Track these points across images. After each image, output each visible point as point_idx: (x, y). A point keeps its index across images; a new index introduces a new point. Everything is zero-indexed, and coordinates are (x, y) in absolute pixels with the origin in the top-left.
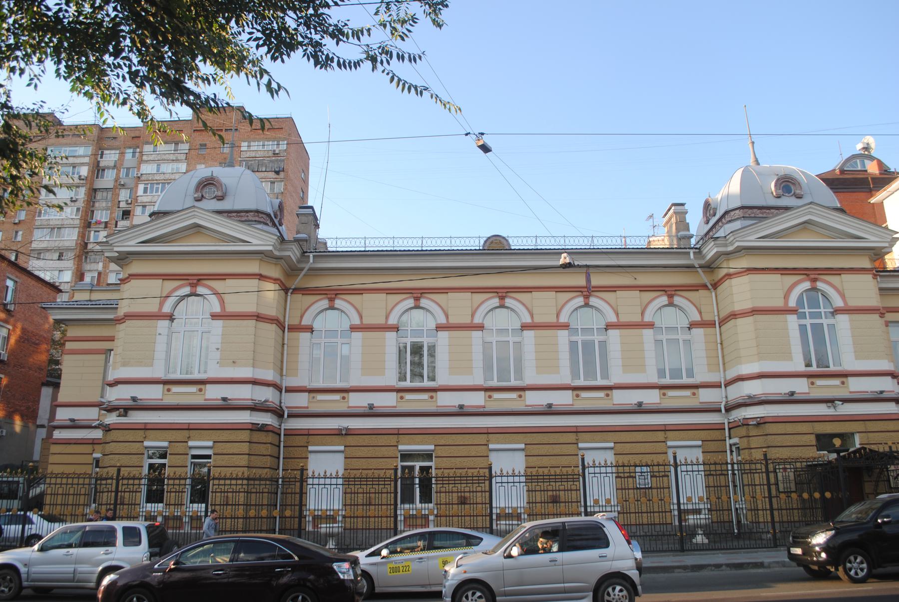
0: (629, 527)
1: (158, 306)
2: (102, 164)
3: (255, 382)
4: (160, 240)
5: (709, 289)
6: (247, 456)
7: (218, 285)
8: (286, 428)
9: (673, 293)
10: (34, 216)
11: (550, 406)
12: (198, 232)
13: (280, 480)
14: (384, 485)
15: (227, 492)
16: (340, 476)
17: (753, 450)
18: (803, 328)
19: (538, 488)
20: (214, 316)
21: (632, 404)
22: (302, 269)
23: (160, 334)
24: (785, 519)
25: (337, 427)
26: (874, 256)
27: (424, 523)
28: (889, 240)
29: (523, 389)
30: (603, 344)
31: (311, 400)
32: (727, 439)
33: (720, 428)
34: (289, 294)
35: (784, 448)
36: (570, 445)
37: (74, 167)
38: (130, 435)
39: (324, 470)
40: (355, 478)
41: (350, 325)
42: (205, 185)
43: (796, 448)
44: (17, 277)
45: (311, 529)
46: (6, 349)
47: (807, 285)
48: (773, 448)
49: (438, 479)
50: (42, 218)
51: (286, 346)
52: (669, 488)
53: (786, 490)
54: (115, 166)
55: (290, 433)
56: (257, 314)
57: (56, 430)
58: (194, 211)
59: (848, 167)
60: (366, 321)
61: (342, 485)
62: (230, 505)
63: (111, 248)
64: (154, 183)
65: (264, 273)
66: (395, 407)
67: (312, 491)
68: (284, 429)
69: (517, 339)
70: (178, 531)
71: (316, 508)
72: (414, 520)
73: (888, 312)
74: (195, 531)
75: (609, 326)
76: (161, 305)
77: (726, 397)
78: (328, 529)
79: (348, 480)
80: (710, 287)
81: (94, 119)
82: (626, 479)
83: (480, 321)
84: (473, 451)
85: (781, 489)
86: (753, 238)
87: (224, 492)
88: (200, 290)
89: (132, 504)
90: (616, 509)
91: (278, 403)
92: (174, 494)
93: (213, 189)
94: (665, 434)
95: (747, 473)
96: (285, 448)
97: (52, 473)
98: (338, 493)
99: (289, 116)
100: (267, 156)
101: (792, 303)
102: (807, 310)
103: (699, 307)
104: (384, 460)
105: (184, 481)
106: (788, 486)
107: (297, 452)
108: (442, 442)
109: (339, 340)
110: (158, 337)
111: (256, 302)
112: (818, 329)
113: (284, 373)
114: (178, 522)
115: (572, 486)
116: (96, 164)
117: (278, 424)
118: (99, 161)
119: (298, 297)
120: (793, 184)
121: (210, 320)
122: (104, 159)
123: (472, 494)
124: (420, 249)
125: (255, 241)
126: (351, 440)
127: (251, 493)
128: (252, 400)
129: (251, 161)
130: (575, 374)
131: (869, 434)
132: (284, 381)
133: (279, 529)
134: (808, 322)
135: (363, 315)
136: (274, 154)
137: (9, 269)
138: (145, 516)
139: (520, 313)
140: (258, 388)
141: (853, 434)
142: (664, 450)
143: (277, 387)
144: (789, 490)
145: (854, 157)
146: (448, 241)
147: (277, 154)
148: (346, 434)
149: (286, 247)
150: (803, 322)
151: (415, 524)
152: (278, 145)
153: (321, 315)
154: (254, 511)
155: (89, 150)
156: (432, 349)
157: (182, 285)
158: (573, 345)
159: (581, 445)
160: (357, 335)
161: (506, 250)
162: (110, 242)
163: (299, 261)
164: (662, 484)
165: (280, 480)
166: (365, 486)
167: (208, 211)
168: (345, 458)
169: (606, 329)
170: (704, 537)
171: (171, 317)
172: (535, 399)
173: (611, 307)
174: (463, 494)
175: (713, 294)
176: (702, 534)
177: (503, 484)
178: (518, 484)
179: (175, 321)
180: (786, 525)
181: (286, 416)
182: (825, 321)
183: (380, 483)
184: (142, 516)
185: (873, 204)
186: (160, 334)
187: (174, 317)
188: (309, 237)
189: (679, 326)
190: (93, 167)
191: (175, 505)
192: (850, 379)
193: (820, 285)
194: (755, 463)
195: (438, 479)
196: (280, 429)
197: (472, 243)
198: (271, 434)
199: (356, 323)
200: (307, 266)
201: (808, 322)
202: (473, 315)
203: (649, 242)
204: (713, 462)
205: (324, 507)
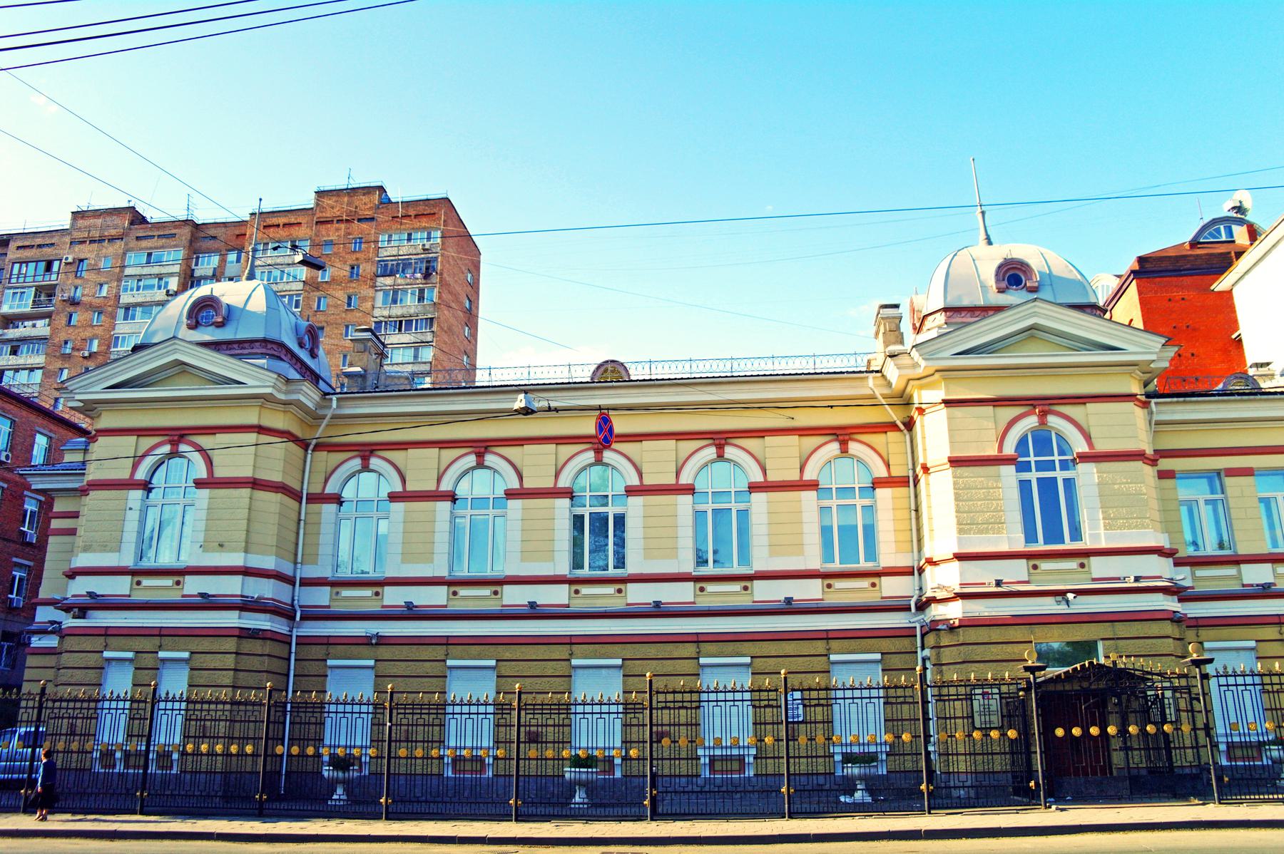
0: (213, 775)
1: (129, 471)
2: (197, 274)
3: (246, 572)
4: (134, 384)
5: (901, 431)
6: (232, 672)
7: (204, 441)
8: (299, 634)
9: (723, 442)
10: (109, 347)
11: (789, 601)
12: (184, 371)
13: (289, 706)
14: (437, 714)
15: (205, 720)
16: (490, 702)
17: (944, 667)
18: (1024, 486)
19: (550, 722)
20: (199, 484)
21: (1252, 585)
22: (323, 417)
23: (131, 509)
24: (980, 768)
25: (364, 634)
26: (1141, 375)
27: (607, 768)
28: (1157, 350)
29: (878, 574)
30: (744, 514)
31: (335, 597)
32: (919, 650)
33: (908, 633)
34: (310, 452)
35: (987, 664)
36: (687, 661)
37: (160, 279)
38: (87, 644)
39: (165, 692)
40: (542, 705)
41: (626, 487)
42: (202, 307)
43: (1004, 664)
44: (51, 431)
45: (450, 774)
46: (37, 527)
47: (1032, 421)
48: (970, 665)
49: (628, 706)
50: (119, 349)
51: (302, 523)
52: (832, 722)
53: (983, 726)
54: (214, 275)
55: (304, 641)
56: (252, 480)
57: (35, 635)
58: (174, 344)
59: (1206, 238)
60: (648, 481)
61: (494, 714)
62: (207, 737)
63: (72, 395)
64: (292, 295)
65: (267, 422)
66: (446, 606)
67: (453, 722)
68: (297, 636)
69: (867, 502)
70: (478, 776)
71: (590, 745)
72: (729, 763)
73: (1161, 457)
74: (160, 772)
75: (877, 483)
76: (135, 467)
77: (921, 589)
78: (573, 774)
79: (629, 708)
80: (902, 427)
81: (186, 213)
82: (677, 711)
83: (690, 482)
84: (550, 668)
85: (977, 725)
86: (98, 388)
87: (201, 720)
88: (183, 448)
89: (85, 735)
90: (884, 749)
91: (289, 601)
92: (138, 721)
93: (212, 313)
94: (828, 643)
95: (961, 700)
96: (298, 662)
97: (29, 693)
98: (487, 725)
99: (444, 196)
100: (415, 252)
101: (1009, 449)
102: (1032, 459)
103: (886, 458)
104: (427, 680)
105: (200, 705)
106: (988, 719)
107: (313, 668)
108: (507, 655)
109: (491, 512)
110: (128, 512)
111: (252, 463)
112: (1048, 486)
113: (299, 560)
114: (479, 764)
115: (312, 719)
116: (189, 273)
117: (288, 629)
118: (194, 270)
119: (322, 455)
120: (1024, 272)
121: (194, 489)
122: (199, 267)
123: (672, 728)
124: (729, 374)
125: (1130, 348)
126: (385, 652)
127: (631, 725)
128: (242, 596)
129: (392, 260)
130: (828, 556)
131: (1119, 641)
132: (298, 571)
133: (286, 771)
134: (1033, 476)
135: (407, 479)
136: (424, 250)
137: (40, 420)
138: (158, 752)
139: (748, 470)
140: (251, 580)
141: (1095, 642)
142: (825, 667)
143: (290, 580)
144: (988, 726)
145: (1215, 222)
146: (687, 365)
147: (427, 250)
148: (376, 644)
149: (294, 387)
150: (1025, 476)
151: (729, 768)
152: (429, 238)
153: (583, 474)
154: (636, 751)
155: (181, 254)
156: (620, 521)
157: (1025, 412)
158: (699, 515)
159: (703, 661)
160: (399, 507)
161: (625, 381)
162: (70, 388)
163: (319, 406)
164: (899, 713)
165: (289, 706)
166: (410, 716)
167: (190, 342)
168: (376, 676)
169: (874, 488)
170: (865, 794)
171: (147, 486)
172: (766, 592)
173: (757, 461)
174: (660, 728)
175: (908, 437)
176: (862, 790)
177: (586, 716)
178: (606, 716)
179: (153, 491)
180: (981, 777)
181: (298, 618)
182: (1060, 475)
183: (431, 711)
184: (97, 750)
185: (1220, 293)
186: (131, 509)
187: (150, 486)
188: (365, 371)
189: (834, 487)
190: (185, 278)
191: (138, 736)
192: (1093, 560)
193: (1052, 420)
194: (957, 686)
195: (628, 706)
196: (291, 636)
197: (721, 367)
198: (268, 642)
199: (514, 487)
200: (329, 413)
201: (1033, 476)
202: (439, 480)
203: (869, 362)
204: (687, 690)
205: (601, 744)
